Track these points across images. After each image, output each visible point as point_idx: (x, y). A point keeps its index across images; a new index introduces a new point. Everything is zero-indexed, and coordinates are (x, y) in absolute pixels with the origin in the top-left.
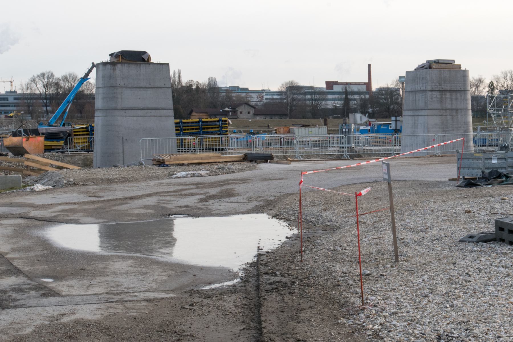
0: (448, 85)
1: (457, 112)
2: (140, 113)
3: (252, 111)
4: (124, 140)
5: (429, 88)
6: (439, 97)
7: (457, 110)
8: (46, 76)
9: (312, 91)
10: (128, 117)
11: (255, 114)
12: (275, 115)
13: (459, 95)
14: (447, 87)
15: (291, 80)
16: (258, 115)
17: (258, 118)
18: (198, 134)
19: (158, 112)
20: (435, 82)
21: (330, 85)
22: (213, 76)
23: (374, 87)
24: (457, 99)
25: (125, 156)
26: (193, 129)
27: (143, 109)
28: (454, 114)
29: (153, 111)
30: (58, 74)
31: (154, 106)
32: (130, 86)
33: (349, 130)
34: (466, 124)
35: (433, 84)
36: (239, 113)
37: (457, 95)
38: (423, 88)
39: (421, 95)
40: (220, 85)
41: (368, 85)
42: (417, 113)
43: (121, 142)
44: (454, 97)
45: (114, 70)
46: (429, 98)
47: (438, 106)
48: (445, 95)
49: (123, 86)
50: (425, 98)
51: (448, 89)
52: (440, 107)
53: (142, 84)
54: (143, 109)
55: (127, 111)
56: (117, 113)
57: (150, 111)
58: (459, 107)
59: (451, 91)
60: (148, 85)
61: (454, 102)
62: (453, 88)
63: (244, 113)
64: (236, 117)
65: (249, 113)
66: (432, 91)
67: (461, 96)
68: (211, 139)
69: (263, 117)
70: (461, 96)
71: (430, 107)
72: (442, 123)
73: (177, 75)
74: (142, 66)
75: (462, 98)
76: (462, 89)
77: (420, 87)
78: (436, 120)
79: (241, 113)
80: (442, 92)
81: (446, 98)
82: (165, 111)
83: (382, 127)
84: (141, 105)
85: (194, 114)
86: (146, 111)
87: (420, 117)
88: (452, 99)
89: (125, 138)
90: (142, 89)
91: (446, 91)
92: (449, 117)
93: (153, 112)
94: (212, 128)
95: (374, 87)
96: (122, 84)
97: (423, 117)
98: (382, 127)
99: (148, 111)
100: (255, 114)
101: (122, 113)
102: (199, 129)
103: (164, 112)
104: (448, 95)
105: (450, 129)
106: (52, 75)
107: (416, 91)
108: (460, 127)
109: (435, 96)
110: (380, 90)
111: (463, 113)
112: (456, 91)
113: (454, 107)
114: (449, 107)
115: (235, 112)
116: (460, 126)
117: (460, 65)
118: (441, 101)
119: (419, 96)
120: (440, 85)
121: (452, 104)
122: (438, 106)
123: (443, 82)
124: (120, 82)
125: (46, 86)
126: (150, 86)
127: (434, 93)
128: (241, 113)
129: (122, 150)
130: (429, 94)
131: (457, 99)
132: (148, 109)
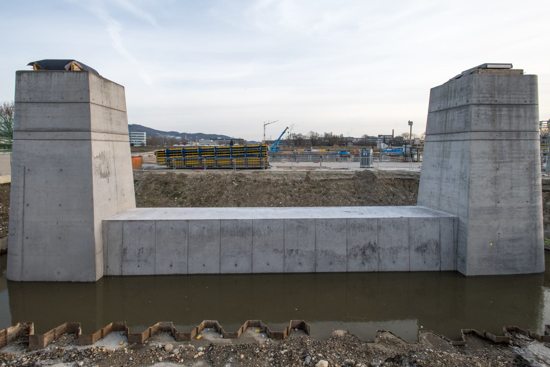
0: (505, 96)
1: (518, 136)
2: (48, 135)
4: (26, 171)
5: (475, 101)
6: (490, 113)
7: (518, 132)
9: (373, 138)
10: (33, 141)
13: (522, 112)
15: (364, 134)
18: (244, 156)
19: (71, 135)
20: (484, 92)
21: (379, 136)
23: (395, 136)
24: (518, 117)
25: (26, 191)
26: (241, 153)
27: (52, 130)
28: (514, 138)
29: (65, 133)
30: (297, 134)
31: (66, 126)
32: (36, 100)
33: (369, 154)
34: (533, 152)
35: (481, 95)
37: (519, 111)
38: (464, 102)
39: (457, 112)
40: (344, 136)
41: (393, 136)
42: (449, 137)
43: (22, 172)
46: (473, 115)
47: (489, 127)
48: (500, 111)
49: (29, 100)
50: (467, 115)
51: (505, 103)
52: (491, 129)
53: (52, 99)
54: (52, 130)
55: (32, 132)
57: (61, 133)
58: (522, 128)
59: (509, 105)
60: (60, 100)
61: (514, 121)
62: (512, 101)
63: (350, 144)
66: (479, 105)
67: (526, 112)
68: (254, 161)
70: (526, 112)
71: (474, 128)
74: (53, 74)
75: (528, 115)
76: (528, 103)
77: (452, 103)
78: (484, 147)
81: (500, 116)
82: (79, 133)
84: (49, 126)
86: (56, 133)
87: (453, 143)
88: (510, 117)
89: (27, 168)
90: (52, 105)
92: (505, 143)
93: (65, 135)
94: (252, 152)
95: (395, 136)
97: (460, 143)
99: (59, 133)
101: (26, 135)
102: (243, 153)
103: (120, 137)
105: (507, 160)
107: (447, 110)
108: (523, 157)
109: (483, 112)
110: (397, 137)
111: (528, 138)
112: (518, 105)
113: (514, 128)
114: (506, 128)
115: (347, 144)
116: (522, 155)
117: (522, 70)
118: (493, 120)
119: (454, 115)
120: (491, 97)
121: (510, 124)
122: (489, 127)
123: (496, 92)
125: (293, 137)
126: (62, 101)
127: (482, 108)
129: (23, 183)
130: (474, 109)
131: (518, 117)
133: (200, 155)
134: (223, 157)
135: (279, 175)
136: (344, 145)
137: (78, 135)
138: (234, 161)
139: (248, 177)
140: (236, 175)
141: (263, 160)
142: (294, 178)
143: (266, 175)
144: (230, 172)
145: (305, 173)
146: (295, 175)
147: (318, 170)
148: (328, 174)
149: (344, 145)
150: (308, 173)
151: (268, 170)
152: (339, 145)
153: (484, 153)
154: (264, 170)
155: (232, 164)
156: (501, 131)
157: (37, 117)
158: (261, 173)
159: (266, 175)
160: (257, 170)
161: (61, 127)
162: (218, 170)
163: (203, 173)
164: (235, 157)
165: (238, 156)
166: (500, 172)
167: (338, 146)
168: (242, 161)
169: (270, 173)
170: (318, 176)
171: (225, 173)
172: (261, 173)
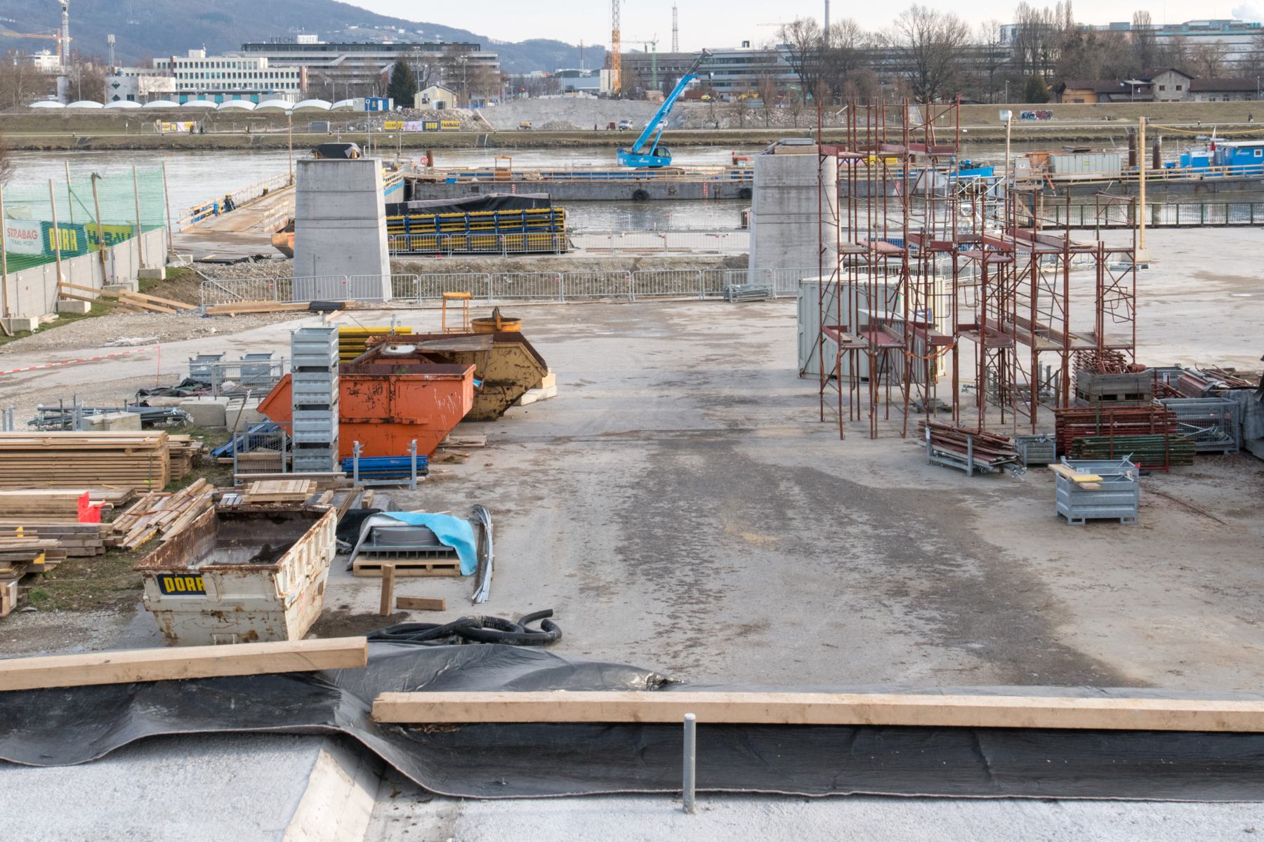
2: (337, 223)
3: (1186, 84)
8: (804, 25)
11: (1191, 91)
12: (1235, 91)
14: (793, 181)
16: (1198, 92)
17: (1198, 99)
18: (520, 230)
22: (1144, 9)
27: (341, 219)
31: (354, 214)
36: (1157, 88)
44: (803, 196)
45: (306, 170)
47: (777, 210)
53: (340, 188)
54: (341, 219)
56: (308, 224)
59: (798, 188)
61: (804, 204)
62: (803, 183)
64: (1150, 97)
65: (1179, 88)
66: (765, 187)
68: (538, 239)
69: (1207, 96)
72: (782, 234)
73: (1064, 11)
79: (1162, 88)
80: (781, 188)
83: (1238, 153)
84: (338, 215)
85: (1067, 91)
88: (799, 200)
91: (791, 187)
92: (793, 226)
96: (315, 188)
98: (1238, 153)
100: (1191, 91)
101: (314, 224)
104: (793, 193)
106: (813, 24)
114: (795, 211)
115: (1149, 87)
118: (781, 202)
122: (777, 210)
124: (312, 186)
127: (769, 191)
128: (1162, 88)
132: (346, 219)
133: (438, 228)
134: (480, 231)
135: (586, 265)
136: (1128, 90)
137: (367, 223)
138: (504, 239)
139: (529, 268)
140: (508, 265)
141: (558, 236)
142: (611, 270)
143: (562, 264)
144: (497, 260)
145: (632, 262)
146: (612, 264)
147: (662, 255)
148: (674, 263)
149: (1128, 90)
150: (637, 260)
151: (566, 255)
152: (1103, 94)
153: (770, 236)
154: (560, 256)
155: (499, 246)
156: (789, 214)
157: (324, 205)
158: (552, 262)
159: (562, 264)
160: (546, 257)
161: (348, 215)
162: (475, 257)
163: (450, 260)
164: (505, 232)
165: (509, 231)
166: (788, 256)
167: (1089, 101)
168: (517, 238)
169: (570, 262)
170: (654, 266)
171: (489, 261)
172: (552, 262)
